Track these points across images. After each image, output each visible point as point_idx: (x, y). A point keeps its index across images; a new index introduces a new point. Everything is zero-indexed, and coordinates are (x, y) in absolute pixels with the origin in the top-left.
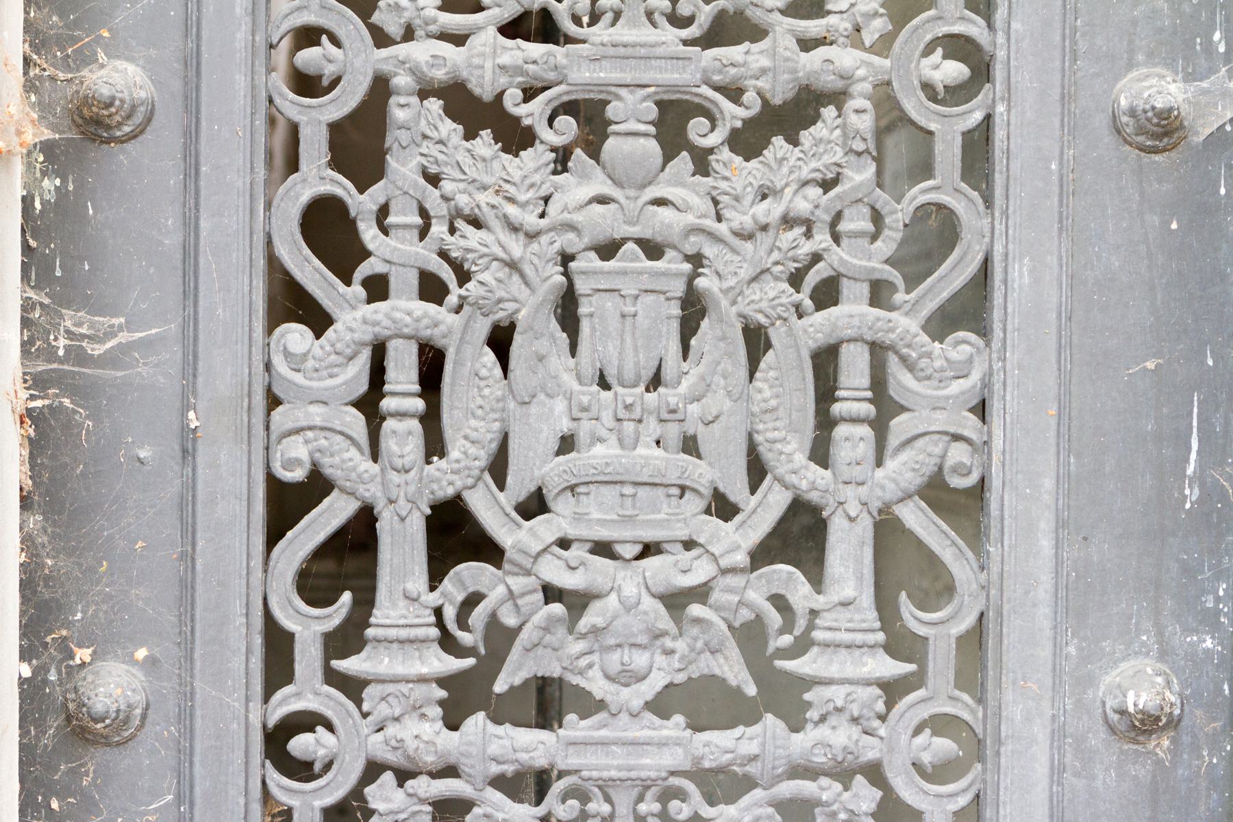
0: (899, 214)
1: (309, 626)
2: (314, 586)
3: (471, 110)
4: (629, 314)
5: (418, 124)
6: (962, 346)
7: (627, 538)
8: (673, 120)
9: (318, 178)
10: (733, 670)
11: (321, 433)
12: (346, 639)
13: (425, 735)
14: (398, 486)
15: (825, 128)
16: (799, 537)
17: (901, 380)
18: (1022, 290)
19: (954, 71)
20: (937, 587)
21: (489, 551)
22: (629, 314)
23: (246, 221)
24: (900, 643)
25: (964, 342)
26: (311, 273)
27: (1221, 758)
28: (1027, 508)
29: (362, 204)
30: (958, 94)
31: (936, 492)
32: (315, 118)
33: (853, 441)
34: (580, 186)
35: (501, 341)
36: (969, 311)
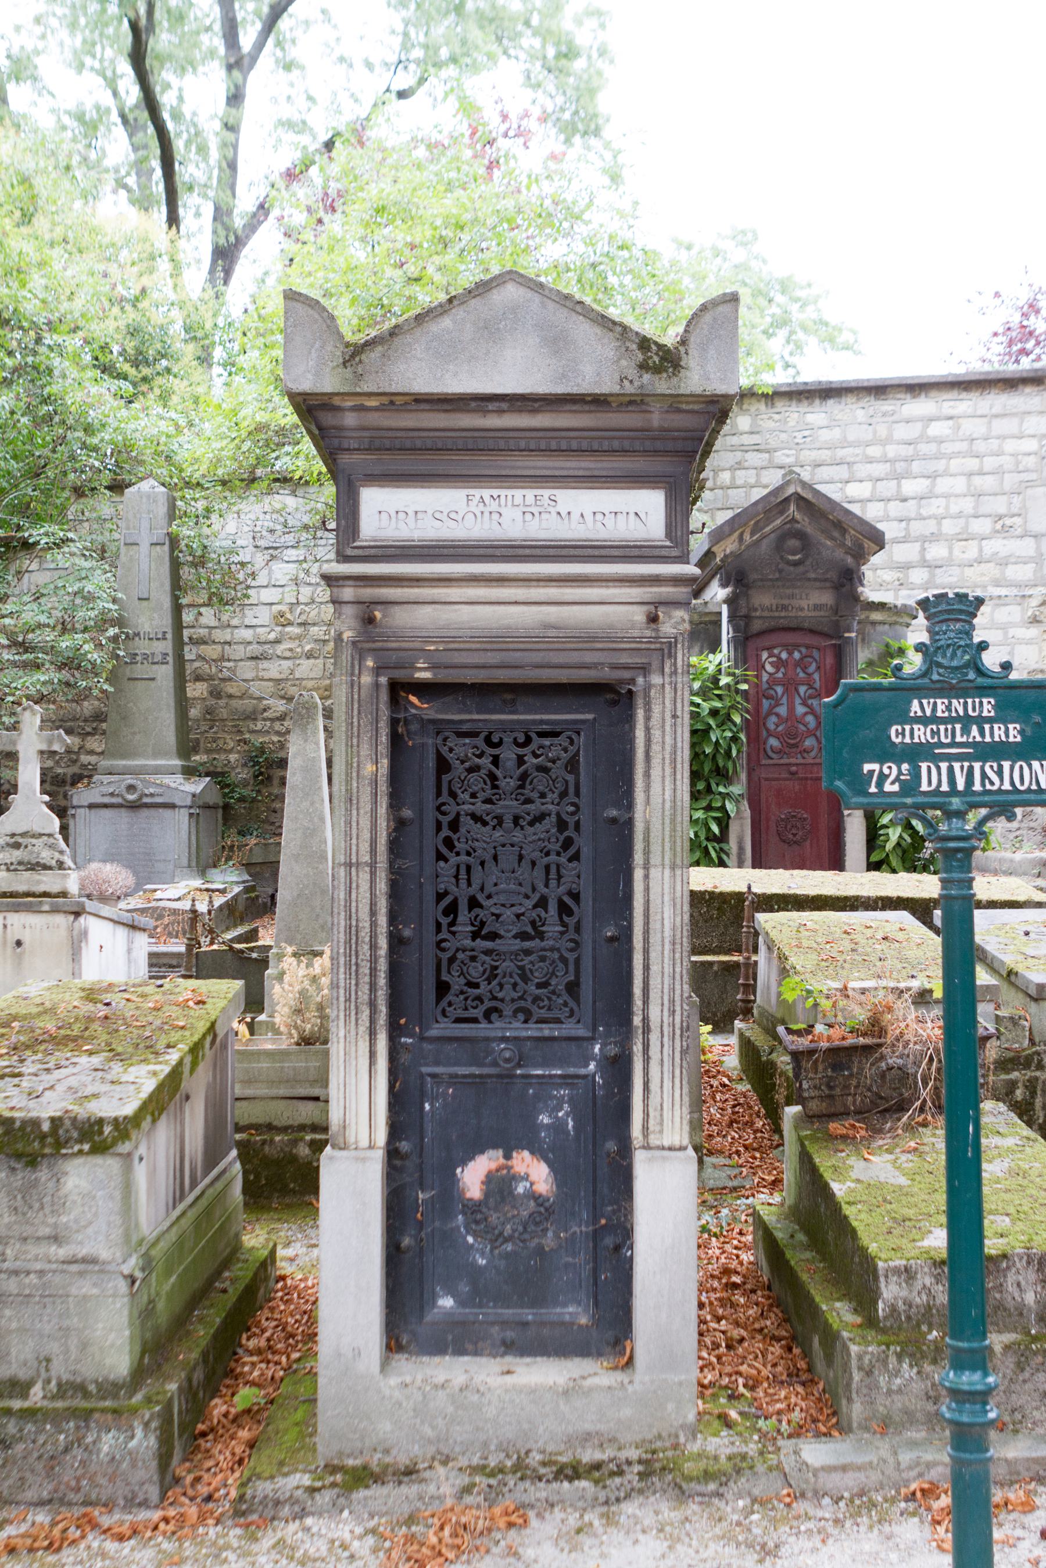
0: (562, 838)
1: (445, 921)
2: (446, 913)
3: (476, 818)
4: (508, 858)
5: (466, 822)
6: (575, 864)
7: (508, 903)
8: (516, 820)
9: (445, 832)
10: (529, 929)
11: (446, 882)
12: (452, 924)
13: (468, 942)
14: (462, 893)
15: (546, 821)
16: (542, 903)
17: (563, 871)
18: (586, 852)
19: (572, 809)
20: (570, 913)
21: (481, 906)
22: (508, 858)
23: (432, 841)
24: (564, 924)
25: (798, 1033)
26: (444, 851)
27: (941, 1327)
28: (587, 897)
29: (455, 837)
30: (573, 814)
31: (570, 893)
32: (445, 820)
33: (553, 883)
34: (497, 834)
35: (482, 864)
36: (576, 857)
